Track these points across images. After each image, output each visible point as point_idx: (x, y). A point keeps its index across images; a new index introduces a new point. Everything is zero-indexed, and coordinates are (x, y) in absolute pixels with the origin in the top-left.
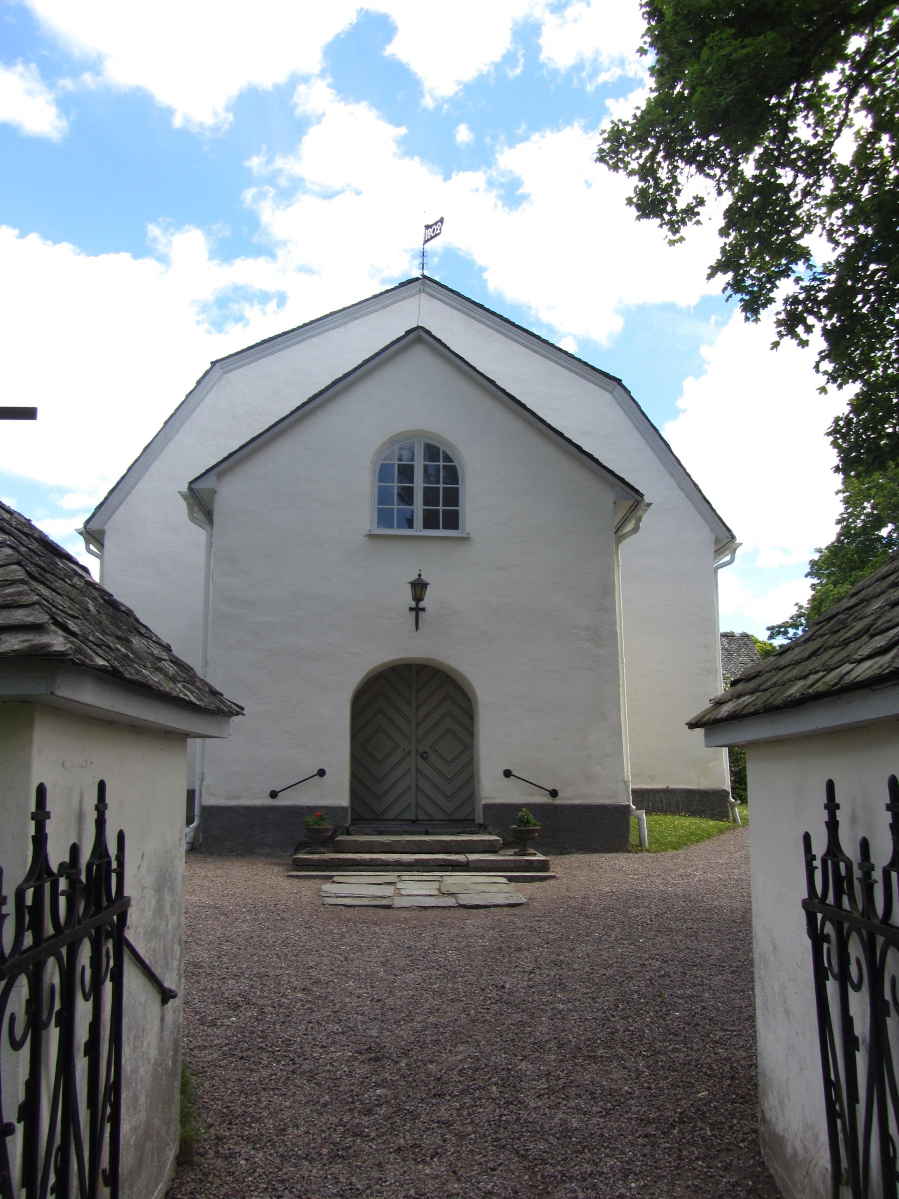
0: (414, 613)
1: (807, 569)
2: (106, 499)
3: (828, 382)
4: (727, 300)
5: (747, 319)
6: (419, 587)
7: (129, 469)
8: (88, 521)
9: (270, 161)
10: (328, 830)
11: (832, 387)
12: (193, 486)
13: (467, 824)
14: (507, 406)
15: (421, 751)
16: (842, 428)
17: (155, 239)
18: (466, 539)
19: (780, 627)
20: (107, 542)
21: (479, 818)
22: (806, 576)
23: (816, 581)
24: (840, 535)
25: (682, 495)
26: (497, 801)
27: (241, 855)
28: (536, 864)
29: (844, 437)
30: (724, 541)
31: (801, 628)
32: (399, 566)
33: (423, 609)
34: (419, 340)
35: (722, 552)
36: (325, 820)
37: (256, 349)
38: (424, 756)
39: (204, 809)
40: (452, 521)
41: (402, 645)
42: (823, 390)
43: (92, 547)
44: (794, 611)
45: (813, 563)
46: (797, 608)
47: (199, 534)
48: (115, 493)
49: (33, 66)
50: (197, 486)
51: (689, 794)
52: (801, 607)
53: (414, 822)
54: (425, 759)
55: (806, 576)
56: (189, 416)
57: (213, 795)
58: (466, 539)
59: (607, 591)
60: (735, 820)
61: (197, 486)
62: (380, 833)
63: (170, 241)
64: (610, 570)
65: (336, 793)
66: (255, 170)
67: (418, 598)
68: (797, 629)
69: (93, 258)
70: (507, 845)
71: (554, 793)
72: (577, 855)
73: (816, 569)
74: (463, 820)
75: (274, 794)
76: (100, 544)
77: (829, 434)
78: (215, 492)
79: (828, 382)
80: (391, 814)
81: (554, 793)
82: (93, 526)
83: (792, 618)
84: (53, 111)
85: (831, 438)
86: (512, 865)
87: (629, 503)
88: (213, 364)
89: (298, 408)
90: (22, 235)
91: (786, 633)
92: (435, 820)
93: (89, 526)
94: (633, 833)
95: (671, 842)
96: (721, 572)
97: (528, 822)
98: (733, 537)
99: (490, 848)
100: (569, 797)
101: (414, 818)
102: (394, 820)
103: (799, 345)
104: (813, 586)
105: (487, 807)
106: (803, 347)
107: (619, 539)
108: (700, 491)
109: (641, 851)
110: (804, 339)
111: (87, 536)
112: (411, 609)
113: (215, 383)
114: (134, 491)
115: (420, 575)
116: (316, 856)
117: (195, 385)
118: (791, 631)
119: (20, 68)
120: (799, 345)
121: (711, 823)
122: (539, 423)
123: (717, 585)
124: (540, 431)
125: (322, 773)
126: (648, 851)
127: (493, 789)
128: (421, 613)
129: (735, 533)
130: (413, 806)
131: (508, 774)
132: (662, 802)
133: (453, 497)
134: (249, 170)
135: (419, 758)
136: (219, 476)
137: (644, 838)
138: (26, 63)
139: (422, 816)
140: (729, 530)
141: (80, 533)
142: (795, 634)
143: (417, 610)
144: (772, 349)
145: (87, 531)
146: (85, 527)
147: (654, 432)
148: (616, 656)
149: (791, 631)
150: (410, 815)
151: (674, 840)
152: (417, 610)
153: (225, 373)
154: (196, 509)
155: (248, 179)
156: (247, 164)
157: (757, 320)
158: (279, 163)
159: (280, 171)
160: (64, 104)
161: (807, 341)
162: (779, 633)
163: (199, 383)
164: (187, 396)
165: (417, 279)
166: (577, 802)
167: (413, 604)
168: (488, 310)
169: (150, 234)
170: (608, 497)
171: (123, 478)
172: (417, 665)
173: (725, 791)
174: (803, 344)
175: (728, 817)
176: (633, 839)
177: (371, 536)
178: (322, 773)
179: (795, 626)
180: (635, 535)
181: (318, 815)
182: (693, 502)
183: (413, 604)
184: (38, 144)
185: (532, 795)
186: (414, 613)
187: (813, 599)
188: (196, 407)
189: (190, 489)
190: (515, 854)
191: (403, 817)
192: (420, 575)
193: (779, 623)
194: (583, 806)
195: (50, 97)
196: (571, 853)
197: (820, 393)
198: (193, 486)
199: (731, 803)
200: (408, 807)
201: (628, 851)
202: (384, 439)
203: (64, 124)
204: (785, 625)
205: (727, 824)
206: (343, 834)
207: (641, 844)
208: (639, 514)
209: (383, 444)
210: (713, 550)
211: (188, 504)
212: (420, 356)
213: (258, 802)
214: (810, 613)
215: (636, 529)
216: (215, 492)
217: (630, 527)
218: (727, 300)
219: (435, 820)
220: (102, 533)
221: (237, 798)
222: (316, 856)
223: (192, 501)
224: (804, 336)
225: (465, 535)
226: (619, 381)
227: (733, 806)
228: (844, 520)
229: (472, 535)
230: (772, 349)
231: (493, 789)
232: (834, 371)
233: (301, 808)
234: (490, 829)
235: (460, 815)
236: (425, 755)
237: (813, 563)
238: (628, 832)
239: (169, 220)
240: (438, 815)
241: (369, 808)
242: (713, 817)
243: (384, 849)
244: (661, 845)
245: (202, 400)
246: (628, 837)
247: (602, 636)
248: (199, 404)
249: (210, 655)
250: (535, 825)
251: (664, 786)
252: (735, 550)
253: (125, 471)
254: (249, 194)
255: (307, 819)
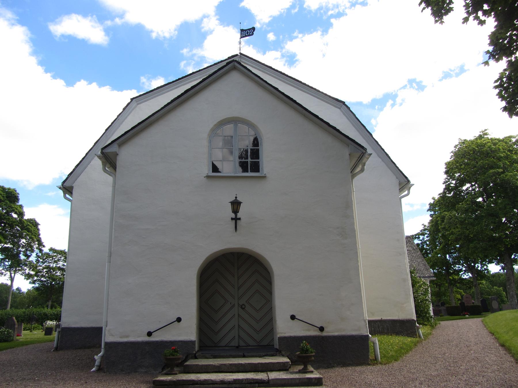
0: (234, 221)
1: (428, 207)
2: (74, 170)
3: (490, 58)
4: (422, 11)
5: (436, 22)
6: (236, 205)
7: (87, 154)
8: (64, 182)
9: (191, 51)
10: (179, 359)
11: (492, 62)
12: (104, 151)
13: (268, 349)
14: (285, 103)
15: (241, 303)
16: (505, 83)
17: (143, 83)
18: (264, 177)
19: (416, 235)
20: (74, 192)
21: (277, 346)
22: (428, 211)
23: (432, 213)
24: (445, 189)
25: (380, 160)
26: (287, 335)
27: (129, 373)
28: (314, 380)
29: (506, 89)
30: (404, 184)
31: (426, 236)
32: (223, 195)
33: (240, 219)
34: (234, 68)
35: (402, 190)
36: (177, 352)
37: (154, 92)
38: (243, 307)
39: (106, 344)
40: (256, 167)
41: (225, 240)
42: (486, 63)
43: (67, 196)
44: (422, 228)
45: (430, 205)
46: (423, 226)
47: (110, 179)
48: (79, 166)
49: (94, 16)
50: (106, 151)
51: (394, 322)
52: (425, 226)
53: (237, 347)
54: (243, 309)
55: (428, 211)
56: (119, 126)
57: (113, 335)
58: (264, 177)
59: (348, 205)
60: (420, 337)
61: (106, 151)
62: (215, 357)
63: (150, 84)
64: (349, 193)
65: (188, 332)
66: (185, 54)
67: (236, 211)
68: (424, 235)
69: (120, 92)
70: (294, 363)
71: (322, 329)
72: (337, 369)
73: (432, 207)
74: (267, 345)
75: (150, 334)
76: (71, 193)
77: (496, 87)
78: (118, 154)
79: (490, 58)
80: (223, 343)
81: (322, 329)
82: (67, 184)
83: (421, 231)
84: (103, 33)
85: (497, 91)
86: (298, 381)
87: (358, 155)
88: (132, 99)
89: (165, 106)
90: (90, 83)
91: (419, 238)
92: (250, 346)
93: (64, 184)
94: (371, 350)
95: (392, 356)
96: (402, 200)
97: (307, 350)
98: (409, 181)
99: (282, 367)
100: (331, 331)
101: (237, 345)
102: (225, 346)
103: (479, 24)
104: (431, 216)
105: (281, 339)
106: (482, 25)
107: (353, 176)
108: (389, 157)
109: (377, 364)
110: (483, 20)
111: (64, 190)
112: (232, 219)
113: (133, 109)
114: (89, 166)
115: (236, 198)
116: (169, 378)
117: (122, 110)
118: (421, 237)
119: (90, 18)
120: (479, 24)
121: (409, 339)
122: (304, 111)
123: (401, 207)
124: (304, 116)
125: (179, 320)
126: (381, 363)
127: (284, 328)
128: (238, 221)
129: (409, 179)
130: (237, 337)
131: (293, 317)
132: (379, 327)
133: (256, 154)
134: (182, 54)
135: (240, 308)
136: (120, 146)
137: (378, 354)
138: (92, 16)
139: (242, 344)
140: (406, 178)
141: (60, 188)
142: (423, 238)
143: (236, 220)
144: (463, 23)
145: (64, 187)
146: (63, 185)
147: (363, 128)
148: (355, 243)
149: (421, 237)
150: (235, 343)
151: (394, 354)
152: (236, 220)
153: (138, 104)
154: (108, 165)
155: (182, 58)
156: (181, 52)
157: (442, 22)
158: (195, 51)
159: (194, 55)
160: (107, 31)
161: (485, 21)
162: (416, 238)
163: (124, 109)
164: (118, 116)
165: (237, 55)
166: (336, 334)
167: (233, 216)
168: (274, 69)
169: (142, 81)
170: (346, 152)
171: (83, 159)
172: (238, 253)
173: (413, 320)
174: (482, 23)
175: (416, 335)
176: (371, 356)
177: (208, 177)
178: (179, 320)
179: (423, 234)
180: (362, 174)
181: (173, 349)
182: (385, 163)
183: (233, 216)
184: (97, 47)
185: (309, 330)
186: (234, 221)
187: (431, 222)
188: (123, 122)
189: (102, 153)
190: (300, 372)
191: (231, 345)
192: (236, 198)
193: (416, 233)
194: (340, 336)
195: (101, 28)
196: (334, 367)
197: (485, 65)
198: (104, 151)
199: (417, 327)
200: (234, 338)
201: (369, 365)
202: (215, 123)
203: (107, 38)
204: (418, 234)
205: (417, 339)
206: (192, 358)
207: (376, 359)
208: (363, 161)
209: (215, 125)
210: (398, 188)
211: (103, 162)
212: (235, 78)
213: (140, 339)
214: (430, 228)
215: (362, 170)
216: (118, 154)
217: (358, 169)
218: (422, 11)
219: (250, 346)
220: (72, 188)
221: (127, 336)
222: (169, 378)
223: (105, 161)
224: (483, 18)
225: (263, 175)
226: (343, 103)
227: (418, 328)
228: (447, 182)
229: (267, 175)
230: (463, 23)
231: (284, 328)
232: (493, 51)
233: (166, 342)
234: (283, 353)
235: (265, 343)
236: (243, 307)
237: (430, 205)
238: (368, 352)
239: (150, 76)
240: (251, 342)
241: (209, 342)
242: (408, 335)
243: (216, 370)
244: (389, 359)
245: (126, 118)
246: (368, 355)
247: (347, 232)
248: (124, 120)
249: (112, 249)
250: (312, 352)
251: (379, 318)
252: (410, 188)
253: (84, 155)
254: (182, 64)
255: (166, 351)
